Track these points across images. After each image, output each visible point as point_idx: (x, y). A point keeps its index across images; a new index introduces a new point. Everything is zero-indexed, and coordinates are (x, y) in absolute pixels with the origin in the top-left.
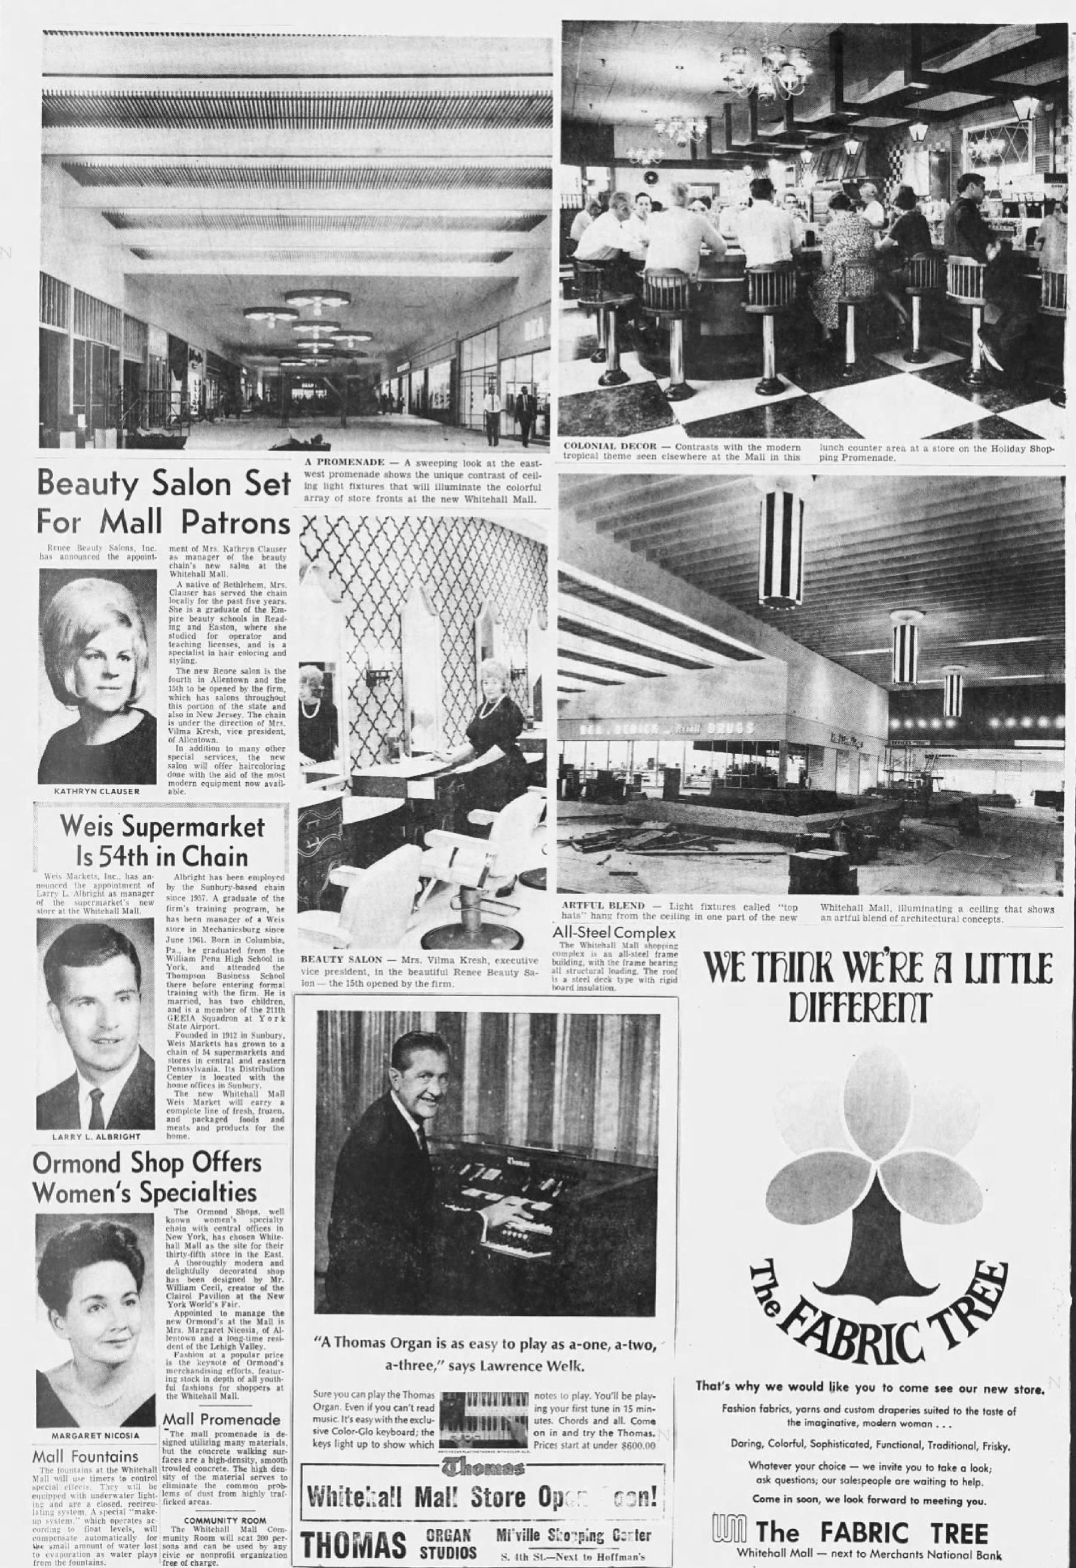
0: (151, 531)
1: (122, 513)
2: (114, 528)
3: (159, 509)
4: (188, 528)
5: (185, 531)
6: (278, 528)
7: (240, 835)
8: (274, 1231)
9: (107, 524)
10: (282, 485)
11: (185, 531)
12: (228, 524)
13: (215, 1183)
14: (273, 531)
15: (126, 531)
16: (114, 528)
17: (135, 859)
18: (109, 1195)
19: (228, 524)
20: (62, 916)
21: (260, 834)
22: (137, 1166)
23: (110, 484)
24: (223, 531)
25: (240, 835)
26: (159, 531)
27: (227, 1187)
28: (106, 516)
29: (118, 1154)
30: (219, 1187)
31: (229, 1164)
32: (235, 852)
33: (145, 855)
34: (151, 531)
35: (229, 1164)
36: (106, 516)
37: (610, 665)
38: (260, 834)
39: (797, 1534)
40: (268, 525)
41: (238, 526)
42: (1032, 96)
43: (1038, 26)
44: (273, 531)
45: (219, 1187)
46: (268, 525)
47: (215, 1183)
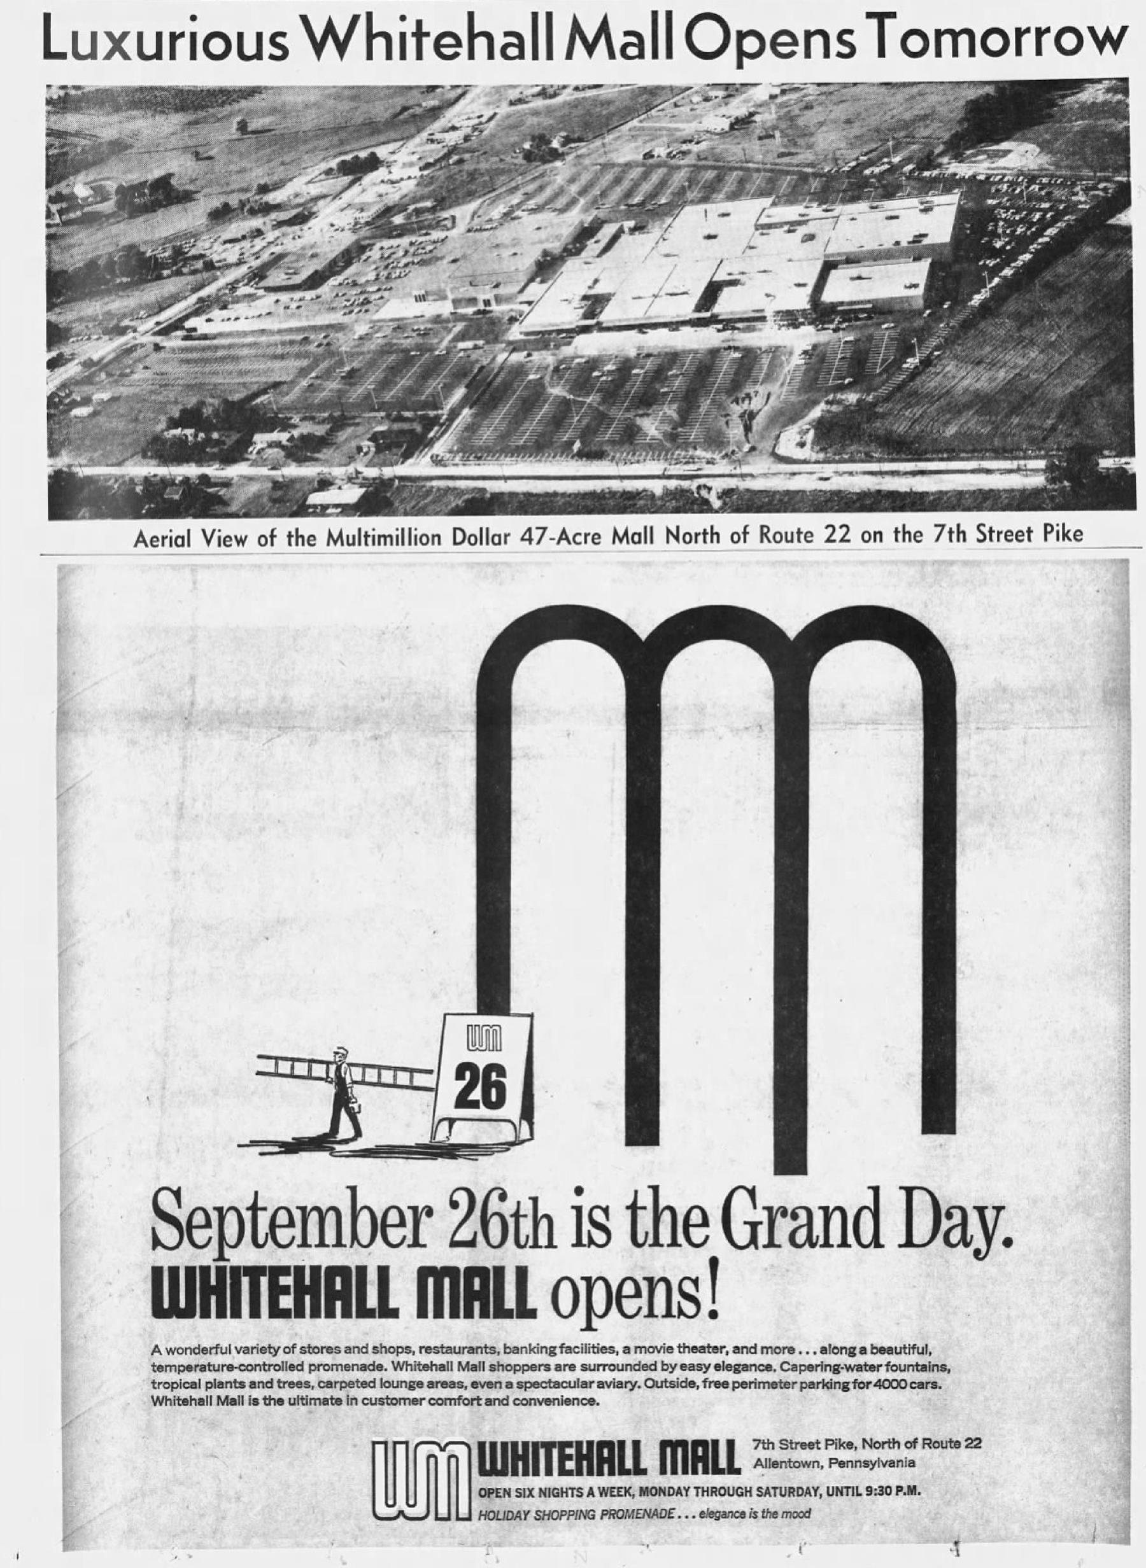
0: (655, 55)
2: (590, 49)
4: (874, 22)
5: (869, 15)
6: (835, 47)
7: (1069, 539)
10: (742, 536)
11: (869, 15)
12: (995, 536)
13: (360, 530)
14: (827, 55)
15: (612, 55)
16: (590, 49)
17: (708, 537)
18: (878, 536)
19: (995, 536)
20: (263, 525)
21: (1029, 540)
22: (981, 537)
23: (796, 536)
24: (955, 53)
25: (1069, 539)
27: (371, 533)
29: (1046, 539)
30: (363, 534)
31: (802, 536)
32: (376, 533)
33: (717, 534)
35: (802, 536)
38: (1029, 540)
39: (599, 537)
40: (817, 42)
41: (1048, 40)
44: (827, 55)
45: (363, 534)
46: (817, 42)
47: (360, 530)
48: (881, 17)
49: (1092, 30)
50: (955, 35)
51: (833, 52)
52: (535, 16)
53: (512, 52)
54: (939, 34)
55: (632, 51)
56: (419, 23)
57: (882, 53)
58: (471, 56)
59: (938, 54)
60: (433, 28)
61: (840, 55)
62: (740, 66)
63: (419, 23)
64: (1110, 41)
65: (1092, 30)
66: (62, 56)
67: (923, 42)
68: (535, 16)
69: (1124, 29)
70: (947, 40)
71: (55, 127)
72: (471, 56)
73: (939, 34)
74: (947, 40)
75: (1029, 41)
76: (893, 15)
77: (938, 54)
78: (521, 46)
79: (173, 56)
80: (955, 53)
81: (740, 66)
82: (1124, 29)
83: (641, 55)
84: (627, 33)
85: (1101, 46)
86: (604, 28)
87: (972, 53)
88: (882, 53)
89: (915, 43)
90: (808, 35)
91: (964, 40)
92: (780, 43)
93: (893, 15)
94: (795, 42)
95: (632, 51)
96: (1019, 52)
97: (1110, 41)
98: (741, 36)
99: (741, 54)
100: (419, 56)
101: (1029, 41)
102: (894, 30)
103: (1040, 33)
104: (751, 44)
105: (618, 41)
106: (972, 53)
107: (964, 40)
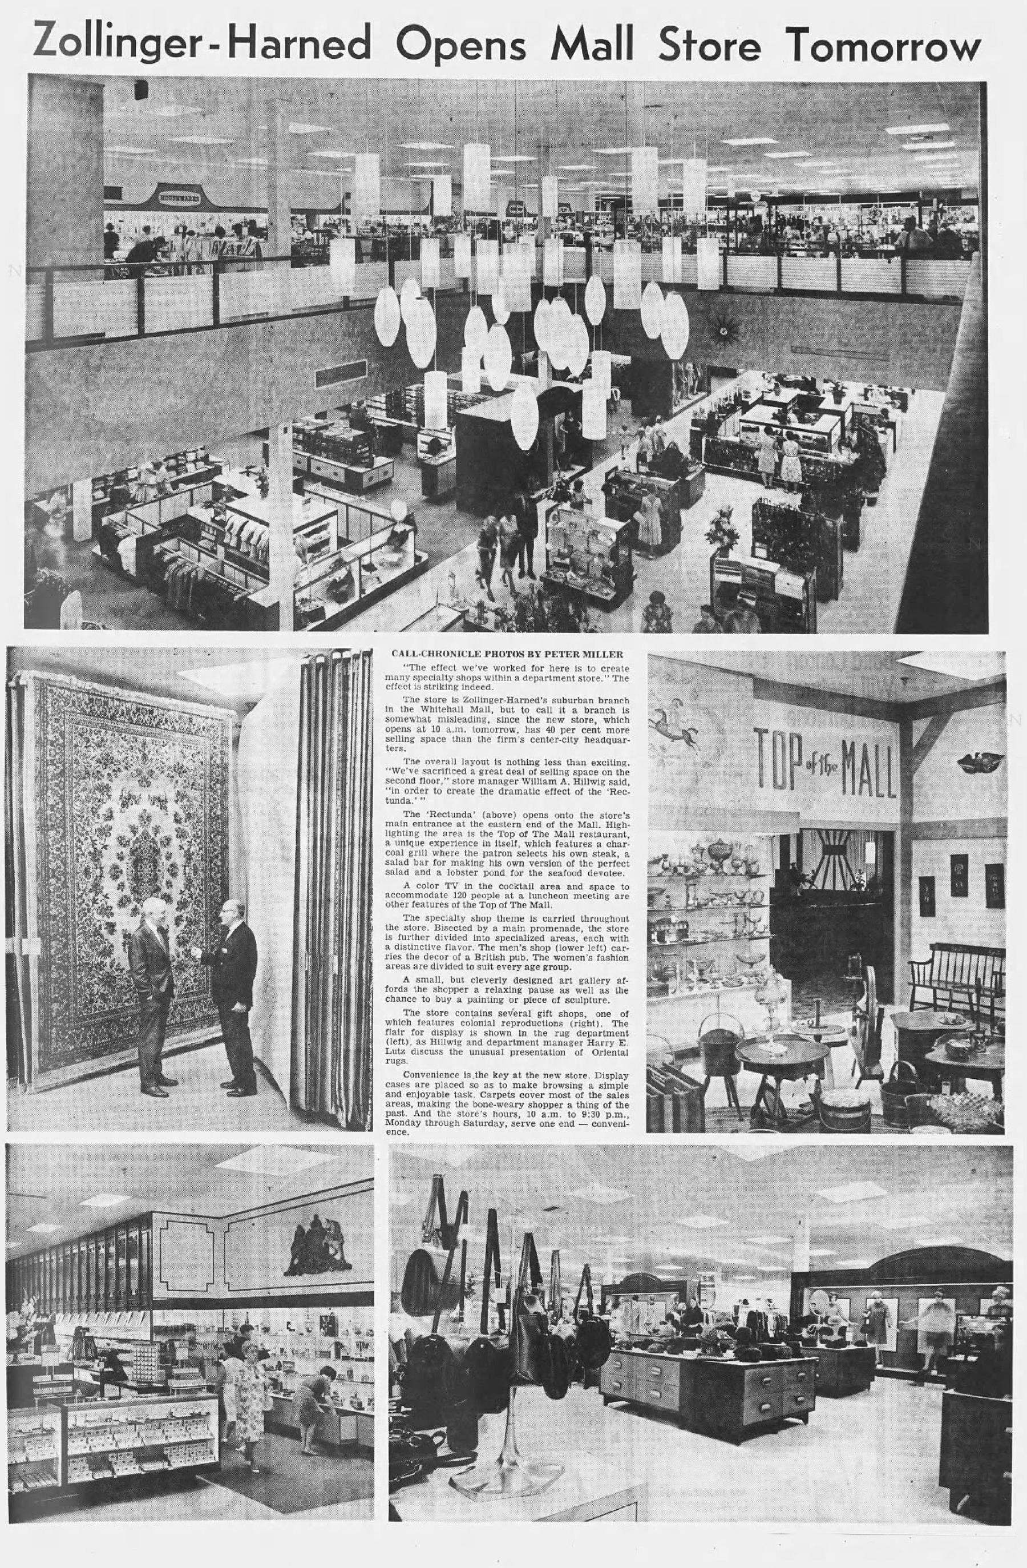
0: (619, 57)
1: (582, 30)
2: (570, 52)
3: (630, 27)
5: (789, 30)
6: (509, 51)
8: (619, 714)
9: (562, 49)
14: (503, 57)
15: (586, 57)
16: (570, 52)
26: (630, 57)
28: (560, 37)
34: (619, 57)
36: (560, 37)
37: (350, 924)
40: (496, 47)
41: (921, 50)
42: (858, 514)
43: (576, 630)
44: (503, 57)
46: (496, 47)
48: (797, 31)
49: (953, 42)
50: (852, 45)
51: (508, 55)
52: (88, 22)
53: (271, 52)
54: (840, 44)
55: (602, 54)
56: (689, 33)
57: (797, 57)
58: (489, 56)
59: (840, 58)
60: (699, 37)
61: (513, 57)
62: (438, 64)
63: (689, 33)
64: (968, 50)
65: (953, 42)
66: (53, 53)
67: (828, 51)
68: (88, 22)
69: (978, 43)
70: (846, 49)
71: (106, 93)
72: (489, 56)
73: (840, 44)
74: (846, 49)
75: (907, 50)
76: (806, 30)
77: (840, 58)
78: (608, 51)
79: (287, 55)
80: (852, 58)
81: (438, 64)
82: (978, 43)
83: (277, 55)
84: (598, 41)
85: (960, 55)
86: (581, 37)
87: (865, 58)
88: (797, 57)
89: (822, 51)
90: (489, 42)
91: (859, 49)
92: (469, 48)
93: (806, 30)
94: (479, 48)
95: (602, 54)
96: (900, 58)
97: (968, 50)
98: (439, 43)
99: (439, 56)
100: (689, 57)
101: (907, 50)
102: (807, 41)
103: (915, 44)
104: (446, 49)
105: (591, 47)
106: (865, 58)
107: (859, 49)
